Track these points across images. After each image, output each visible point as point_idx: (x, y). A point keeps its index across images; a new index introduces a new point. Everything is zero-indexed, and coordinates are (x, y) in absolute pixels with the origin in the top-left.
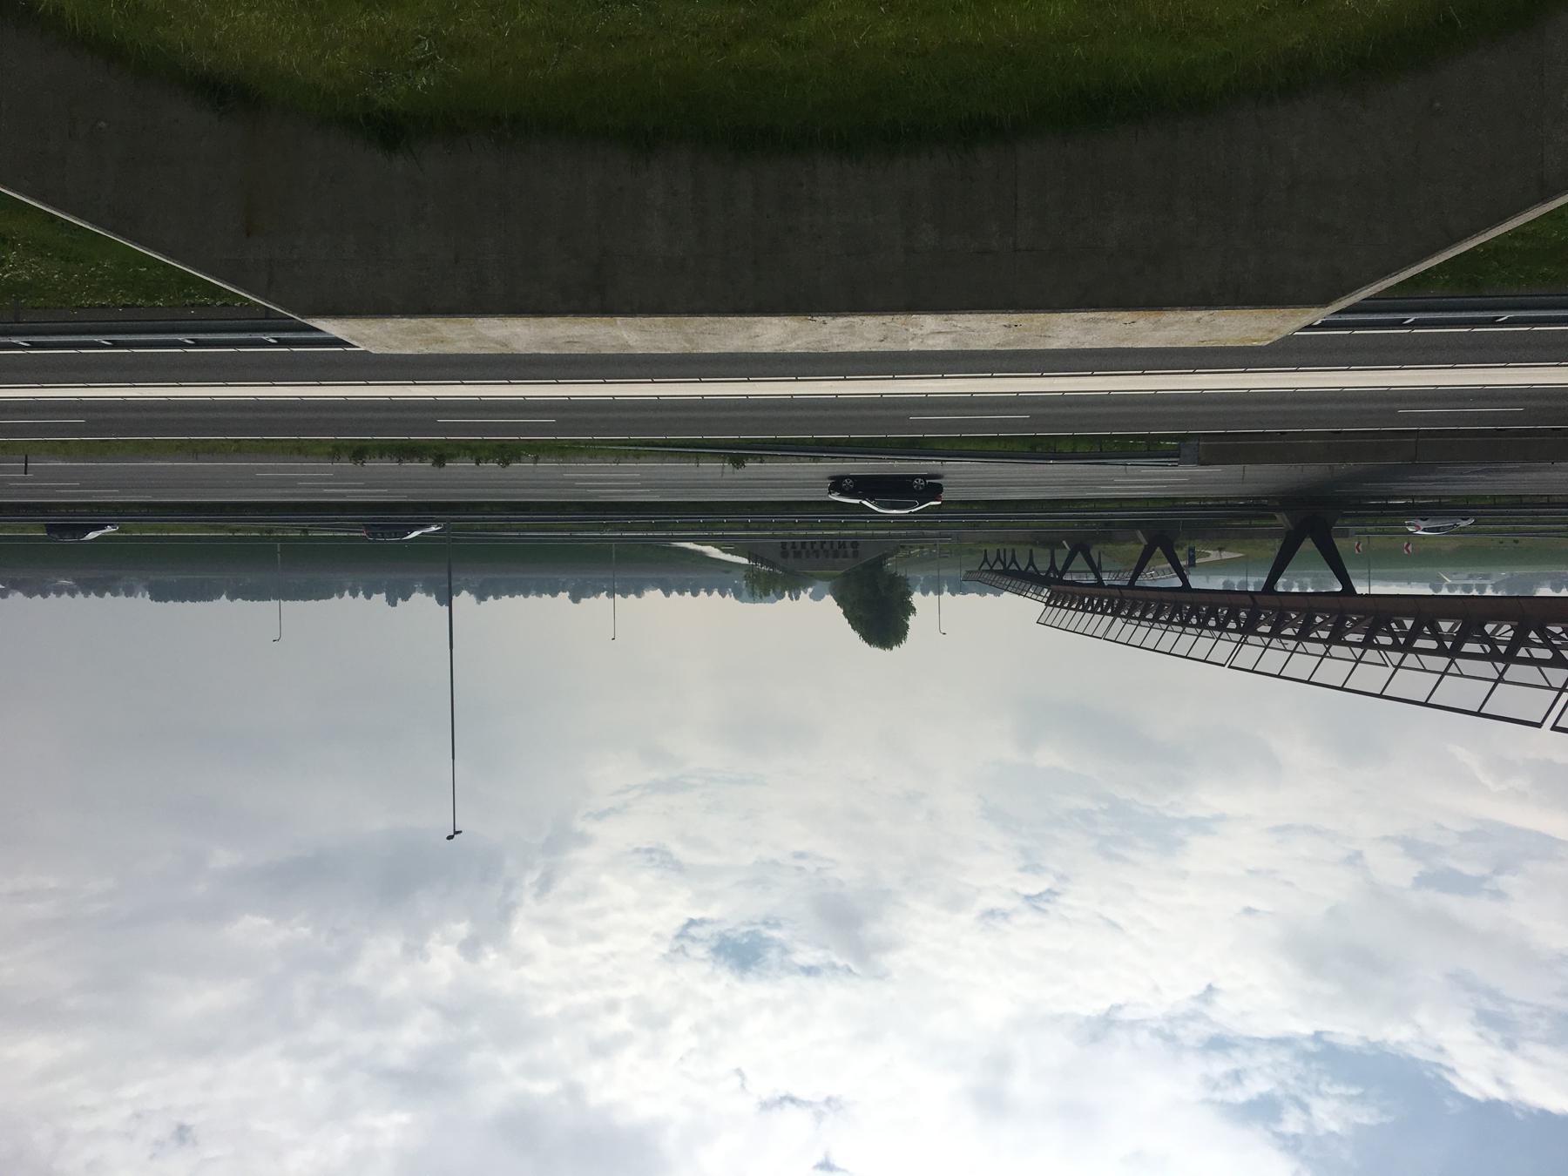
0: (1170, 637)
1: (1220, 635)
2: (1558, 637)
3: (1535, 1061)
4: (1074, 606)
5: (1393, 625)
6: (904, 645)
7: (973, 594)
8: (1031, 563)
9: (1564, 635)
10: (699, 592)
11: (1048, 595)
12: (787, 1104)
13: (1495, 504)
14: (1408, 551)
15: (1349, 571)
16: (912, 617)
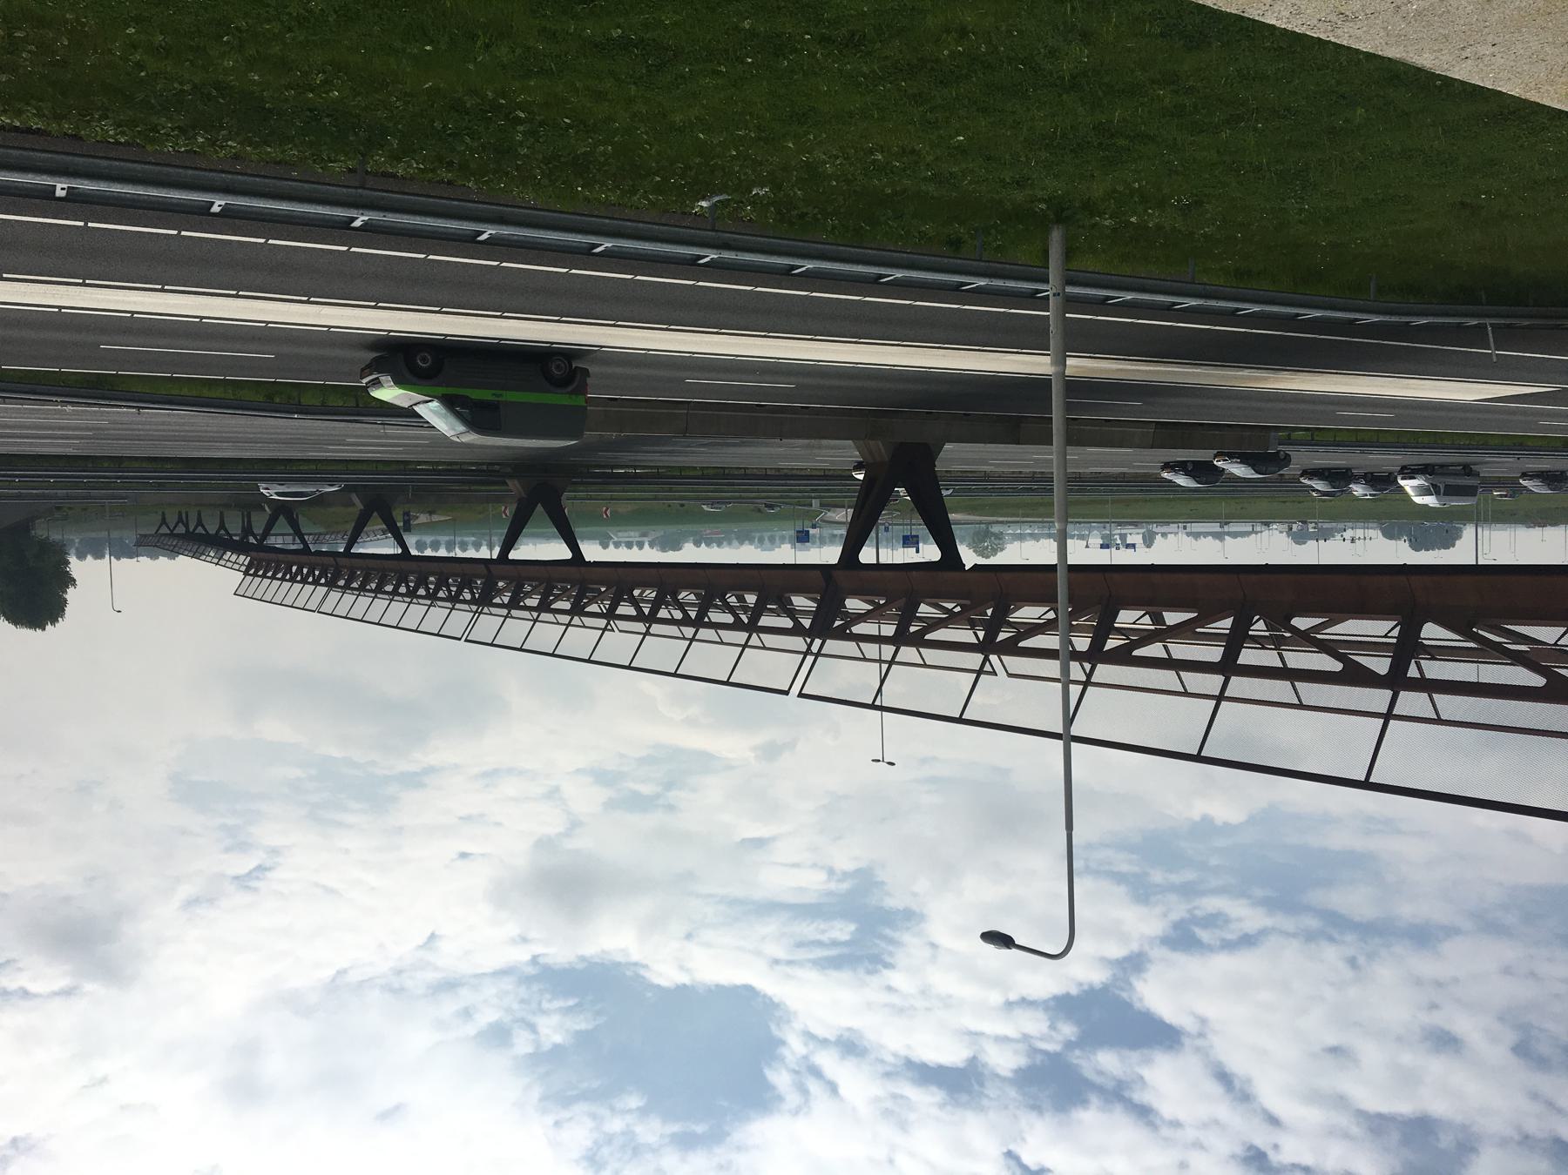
1: (538, 616)
3: (708, 945)
4: (279, 576)
6: (61, 623)
8: (222, 526)
11: (246, 563)
13: (724, 474)
14: (606, 515)
16: (70, 590)
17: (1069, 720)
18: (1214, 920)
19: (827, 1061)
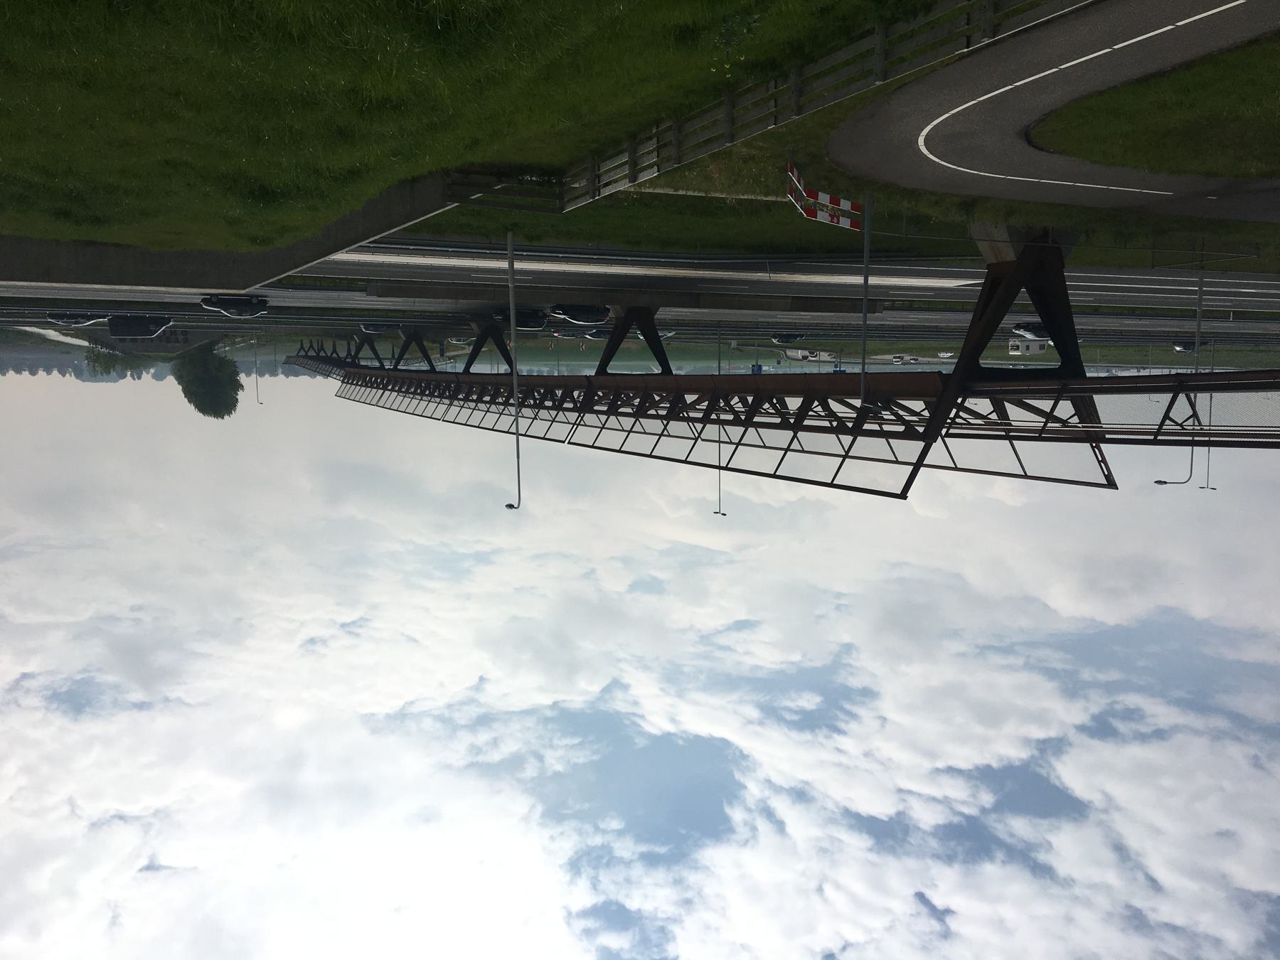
0: (466, 412)
3: (696, 703)
5: (536, 394)
7: (304, 376)
8: (334, 351)
10: (52, 371)
12: (117, 821)
16: (240, 393)
18: (1132, 714)
19: (782, 806)
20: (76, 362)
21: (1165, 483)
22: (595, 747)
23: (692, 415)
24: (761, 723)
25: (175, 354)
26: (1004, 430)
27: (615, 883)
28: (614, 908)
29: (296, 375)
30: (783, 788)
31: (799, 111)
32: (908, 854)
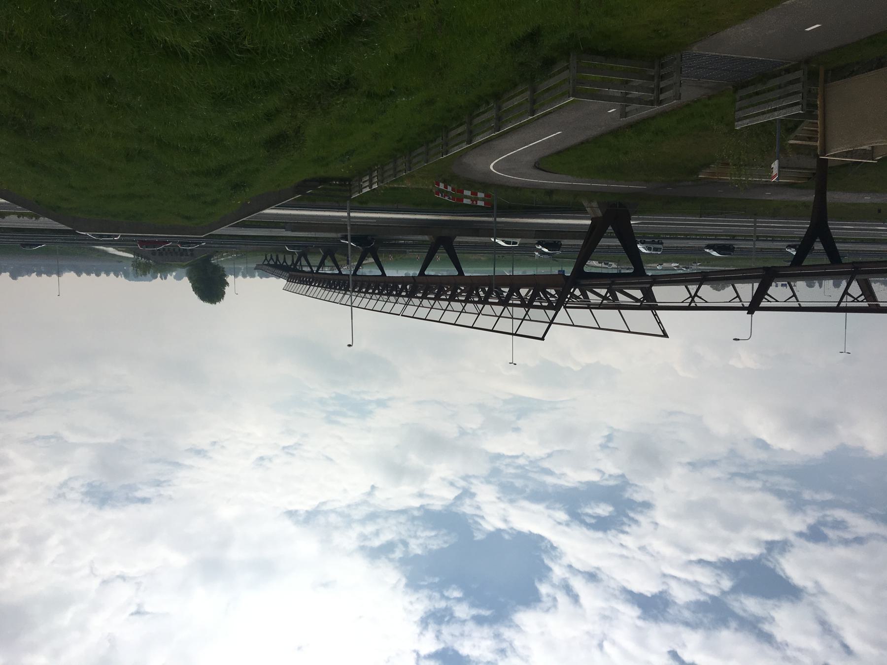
2: (553, 296)
3: (522, 509)
8: (285, 261)
9: (556, 295)
15: (463, 269)
16: (227, 288)
17: (352, 303)
18: (839, 525)
19: (578, 585)
20: (125, 268)
21: (739, 340)
22: (446, 538)
23: (460, 298)
24: (568, 525)
25: (187, 263)
26: (587, 304)
27: (453, 635)
28: (450, 653)
29: (267, 277)
30: (579, 571)
31: (427, 161)
32: (667, 621)
